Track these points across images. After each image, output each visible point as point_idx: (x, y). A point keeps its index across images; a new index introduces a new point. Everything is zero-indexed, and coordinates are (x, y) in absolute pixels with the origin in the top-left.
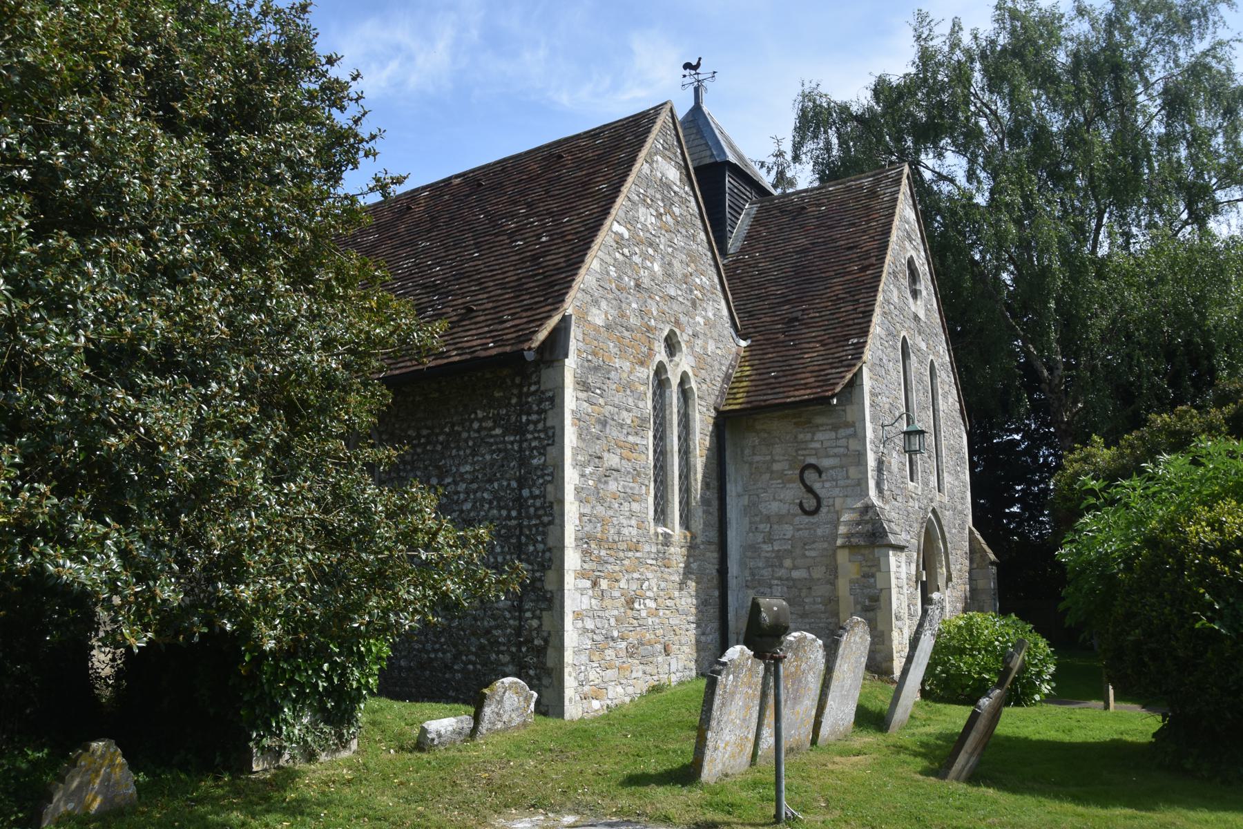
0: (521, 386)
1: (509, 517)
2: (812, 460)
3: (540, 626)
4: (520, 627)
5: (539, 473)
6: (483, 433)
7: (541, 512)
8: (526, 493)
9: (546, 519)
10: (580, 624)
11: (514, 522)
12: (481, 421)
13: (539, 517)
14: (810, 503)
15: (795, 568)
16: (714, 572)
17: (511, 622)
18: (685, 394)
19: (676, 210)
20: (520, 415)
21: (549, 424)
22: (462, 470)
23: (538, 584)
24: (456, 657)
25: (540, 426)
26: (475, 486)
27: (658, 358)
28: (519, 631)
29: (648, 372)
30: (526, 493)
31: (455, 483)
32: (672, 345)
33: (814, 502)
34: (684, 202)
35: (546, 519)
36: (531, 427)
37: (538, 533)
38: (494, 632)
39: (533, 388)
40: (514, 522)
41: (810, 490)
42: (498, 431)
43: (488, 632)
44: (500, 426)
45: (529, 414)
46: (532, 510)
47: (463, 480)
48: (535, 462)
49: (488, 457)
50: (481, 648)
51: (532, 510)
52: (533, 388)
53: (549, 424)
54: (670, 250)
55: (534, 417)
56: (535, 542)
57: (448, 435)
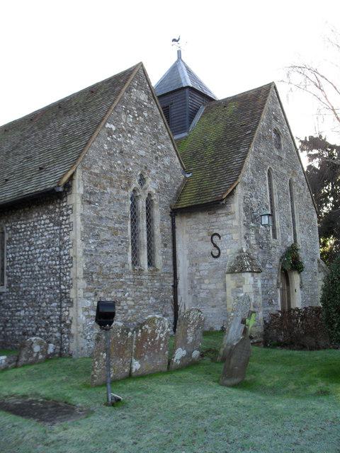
0: (60, 204)
1: (56, 265)
2: (216, 231)
3: (69, 314)
4: (60, 316)
5: (67, 243)
6: (46, 226)
7: (68, 262)
8: (62, 253)
9: (70, 265)
10: (87, 313)
11: (58, 267)
12: (44, 220)
13: (67, 264)
14: (216, 252)
15: (210, 283)
16: (171, 287)
17: (58, 313)
18: (149, 204)
19: (146, 114)
20: (59, 217)
21: (71, 220)
22: (38, 243)
23: (67, 295)
24: (37, 329)
25: (67, 222)
26: (43, 250)
27: (134, 186)
28: (60, 316)
29: (129, 193)
30: (62, 253)
31: (35, 249)
32: (142, 180)
33: (217, 251)
34: (150, 110)
35: (70, 265)
36: (63, 223)
37: (67, 271)
38: (51, 317)
39: (64, 204)
40: (58, 267)
41: (215, 246)
42: (51, 225)
43: (48, 318)
44: (52, 222)
45: (63, 216)
46: (64, 261)
47: (38, 248)
48: (65, 238)
49: (48, 237)
50: (47, 325)
51: (64, 261)
52: (64, 204)
53: (71, 220)
54: (141, 134)
55: (65, 218)
56: (66, 275)
57: (32, 227)
